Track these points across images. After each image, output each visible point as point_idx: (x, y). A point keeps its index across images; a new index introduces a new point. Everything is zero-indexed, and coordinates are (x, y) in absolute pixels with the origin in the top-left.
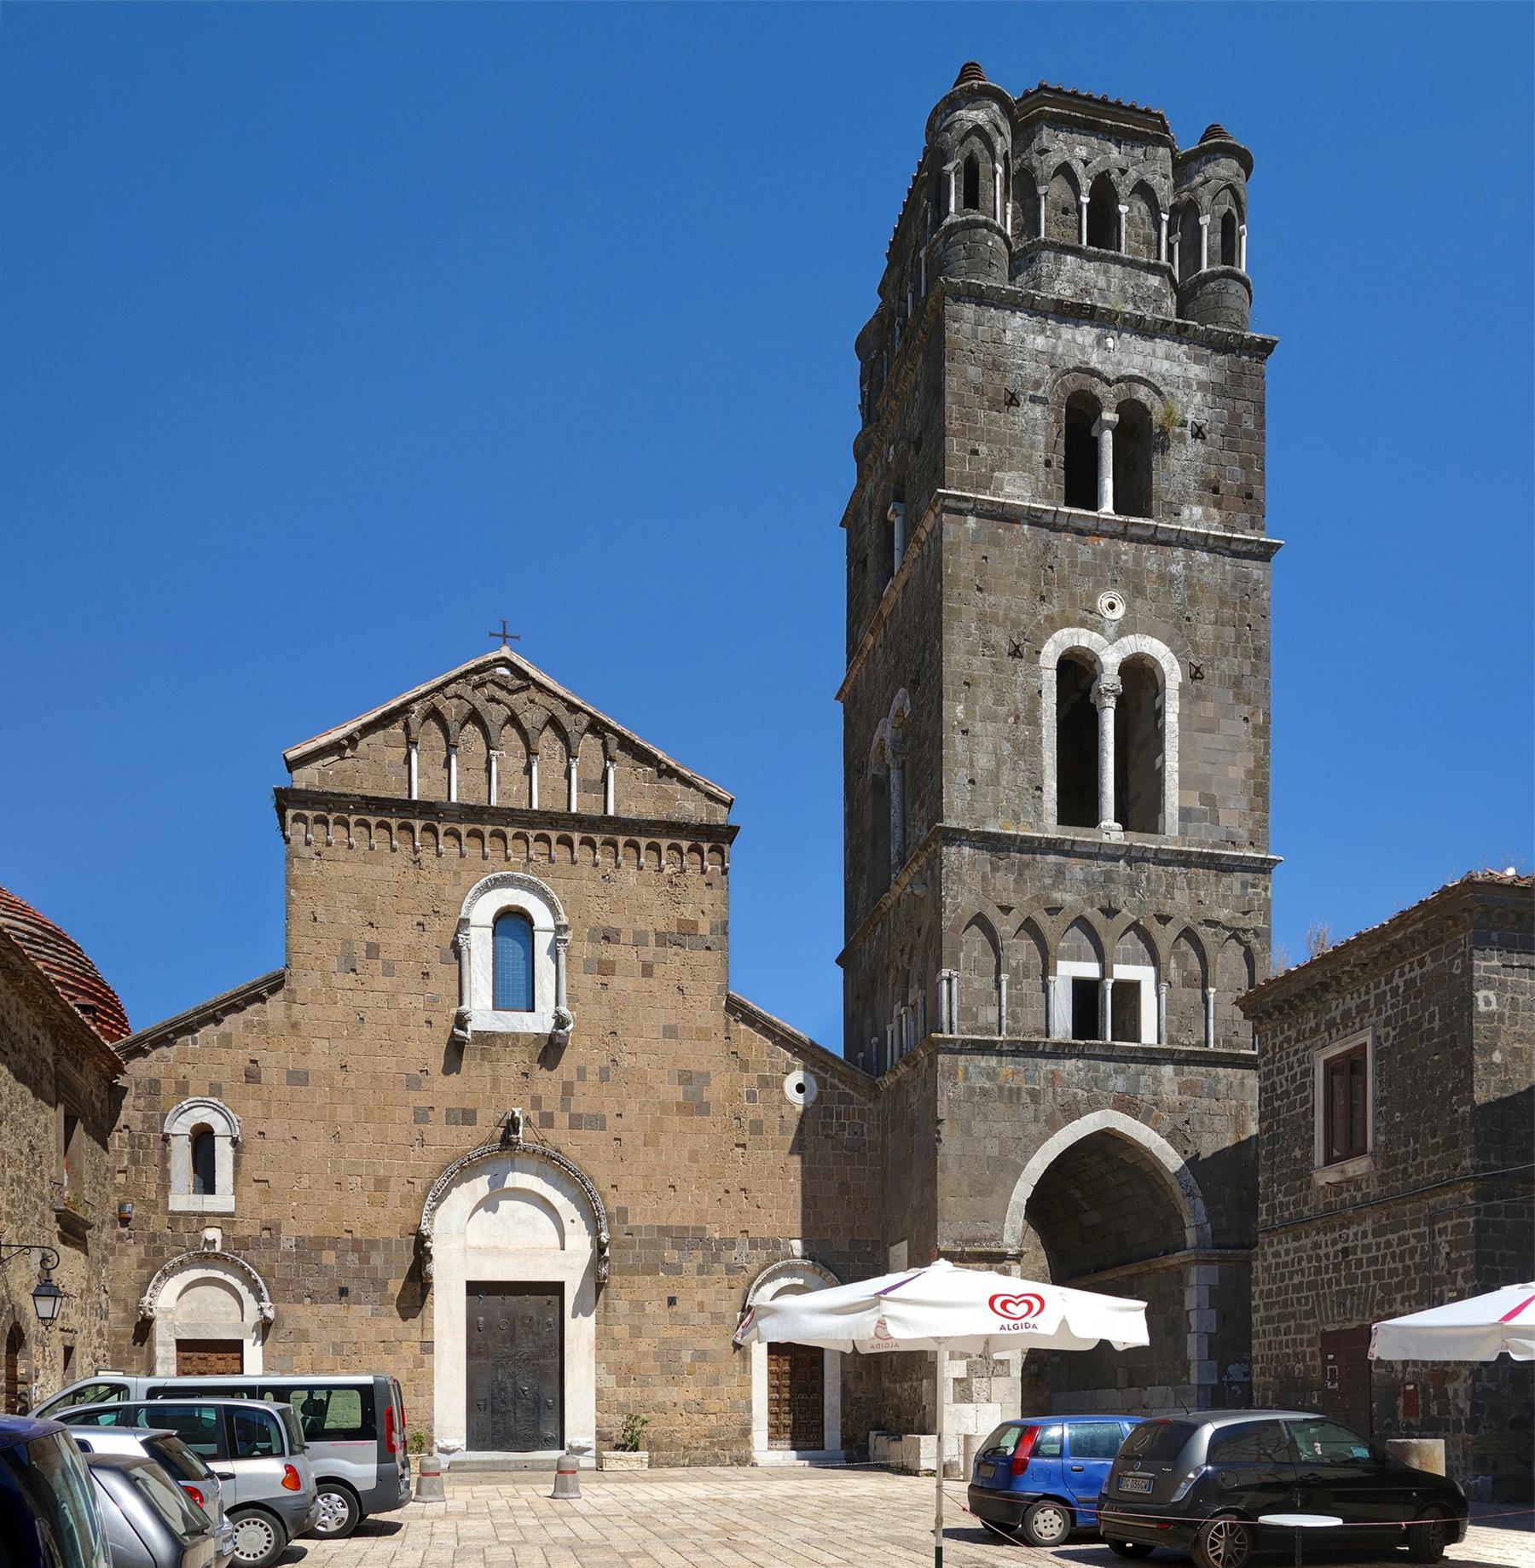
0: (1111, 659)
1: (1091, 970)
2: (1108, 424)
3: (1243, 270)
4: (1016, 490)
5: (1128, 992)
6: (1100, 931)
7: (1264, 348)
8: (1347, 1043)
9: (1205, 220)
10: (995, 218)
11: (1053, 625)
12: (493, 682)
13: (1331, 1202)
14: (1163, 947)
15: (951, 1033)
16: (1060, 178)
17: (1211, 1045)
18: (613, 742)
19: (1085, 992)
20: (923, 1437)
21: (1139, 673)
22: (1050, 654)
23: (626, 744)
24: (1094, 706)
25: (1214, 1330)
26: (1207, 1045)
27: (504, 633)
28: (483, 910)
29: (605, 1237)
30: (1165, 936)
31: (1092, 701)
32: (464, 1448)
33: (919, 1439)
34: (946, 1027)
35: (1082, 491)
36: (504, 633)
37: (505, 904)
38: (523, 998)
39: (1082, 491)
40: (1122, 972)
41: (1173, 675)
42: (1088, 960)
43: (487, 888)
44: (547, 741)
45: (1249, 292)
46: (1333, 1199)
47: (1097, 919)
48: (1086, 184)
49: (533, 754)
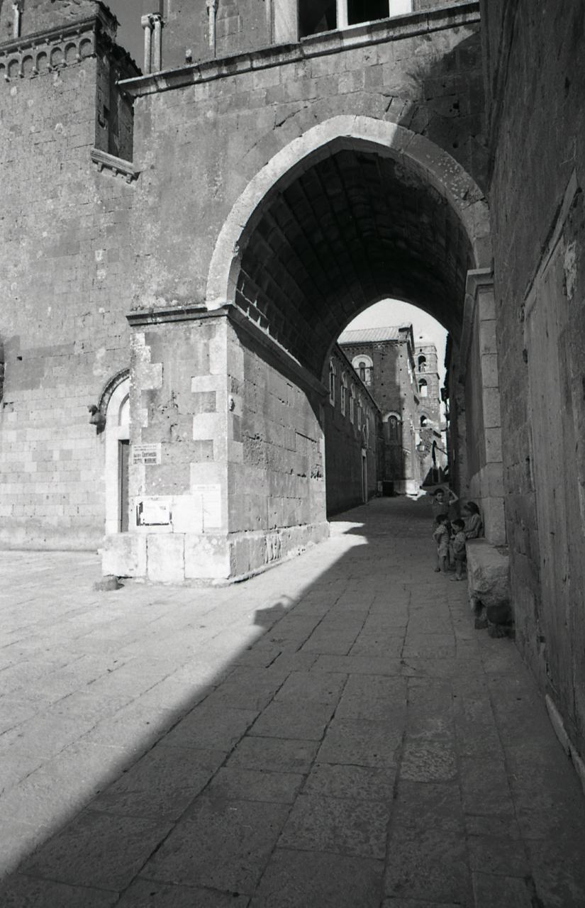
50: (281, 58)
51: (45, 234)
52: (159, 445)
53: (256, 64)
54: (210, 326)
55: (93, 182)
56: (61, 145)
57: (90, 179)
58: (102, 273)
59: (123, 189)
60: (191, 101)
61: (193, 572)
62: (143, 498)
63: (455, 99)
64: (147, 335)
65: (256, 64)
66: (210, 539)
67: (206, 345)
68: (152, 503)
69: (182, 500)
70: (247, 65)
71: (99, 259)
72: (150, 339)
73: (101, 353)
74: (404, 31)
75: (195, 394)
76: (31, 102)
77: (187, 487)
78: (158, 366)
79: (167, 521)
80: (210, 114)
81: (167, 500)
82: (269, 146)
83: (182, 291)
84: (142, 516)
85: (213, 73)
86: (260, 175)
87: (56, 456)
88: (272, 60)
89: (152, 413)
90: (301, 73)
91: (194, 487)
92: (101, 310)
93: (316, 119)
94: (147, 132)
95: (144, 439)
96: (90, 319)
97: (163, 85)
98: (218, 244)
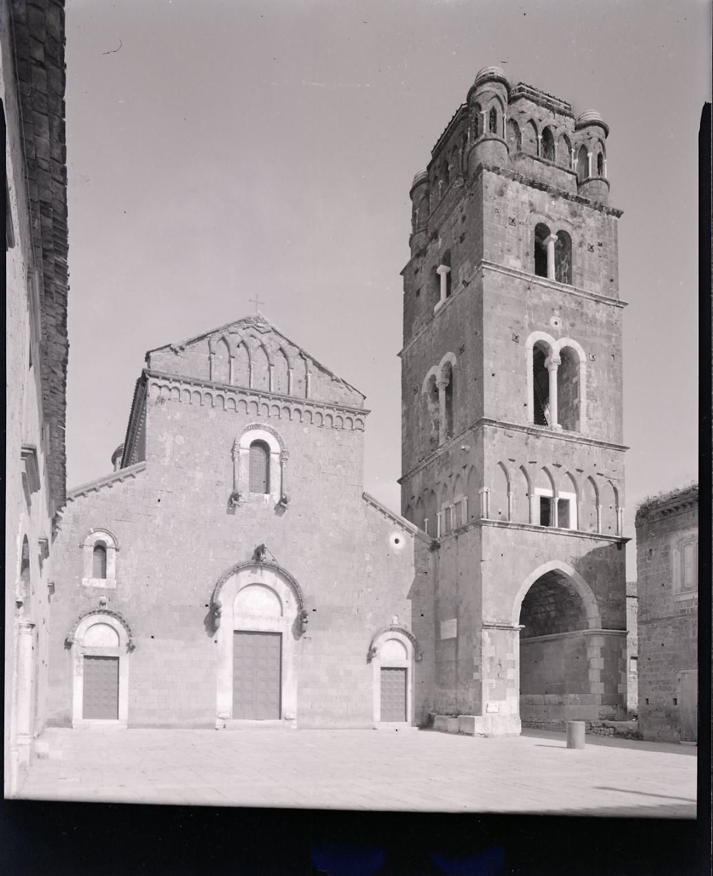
0: (556, 347)
1: (548, 493)
2: (553, 239)
3: (606, 177)
4: (514, 263)
5: (564, 504)
6: (576, 478)
7: (618, 214)
8: (403, 521)
9: (590, 155)
10: (504, 138)
11: (533, 328)
12: (252, 327)
13: (685, 610)
14: (579, 484)
15: (487, 518)
16: (529, 123)
17: (600, 532)
18: (310, 362)
19: (545, 502)
20: (476, 717)
21: (566, 354)
22: (530, 342)
23: (316, 364)
24: (547, 369)
25: (603, 668)
26: (598, 532)
27: (257, 304)
28: (246, 440)
29: (642, 649)
30: (582, 479)
31: (545, 366)
32: (232, 717)
33: (474, 718)
34: (485, 515)
35: (541, 269)
36: (257, 304)
37: (257, 438)
38: (263, 486)
39: (541, 269)
40: (563, 495)
41: (582, 355)
42: (549, 488)
43: (248, 429)
44: (278, 359)
45: (609, 188)
46: (686, 608)
47: (551, 469)
48: (540, 130)
49: (272, 365)
50: (540, 530)
51: (331, 534)
52: (494, 680)
53: (531, 529)
54: (513, 634)
55: (363, 510)
56: (471, 551)
57: (361, 508)
58: (369, 568)
59: (382, 520)
60: (505, 534)
61: (510, 732)
62: (488, 702)
63: (590, 565)
64: (489, 633)
65: (531, 529)
66: (515, 718)
67: (512, 641)
68: (492, 704)
69: (503, 702)
70: (528, 529)
71: (368, 559)
72: (490, 635)
73: (370, 615)
74: (578, 536)
75: (508, 661)
76: (319, 443)
77: (505, 698)
78: (493, 647)
79: (497, 711)
80: (513, 544)
81: (497, 703)
82: (534, 565)
83: (503, 617)
84: (488, 709)
85: (516, 527)
86: (531, 575)
87: (342, 673)
88: (536, 530)
89: (491, 667)
90: (545, 538)
91: (508, 698)
92: (369, 590)
93: (550, 559)
94: (488, 544)
95: (488, 678)
96: (362, 595)
97: (496, 525)
98: (516, 600)
